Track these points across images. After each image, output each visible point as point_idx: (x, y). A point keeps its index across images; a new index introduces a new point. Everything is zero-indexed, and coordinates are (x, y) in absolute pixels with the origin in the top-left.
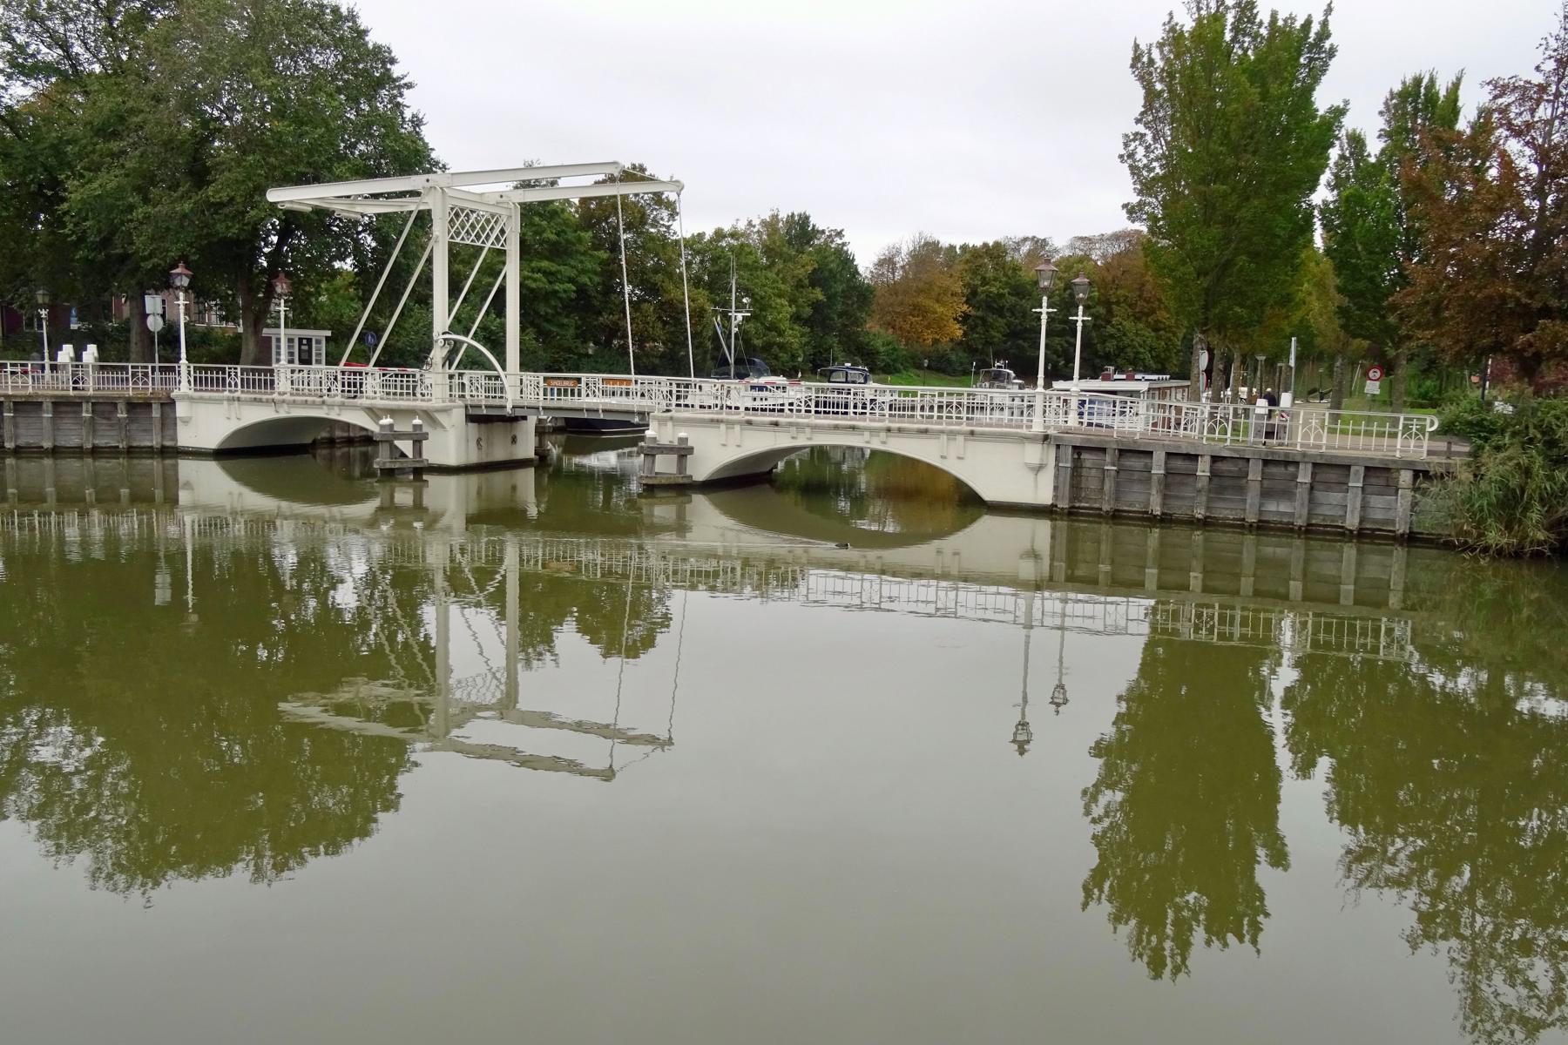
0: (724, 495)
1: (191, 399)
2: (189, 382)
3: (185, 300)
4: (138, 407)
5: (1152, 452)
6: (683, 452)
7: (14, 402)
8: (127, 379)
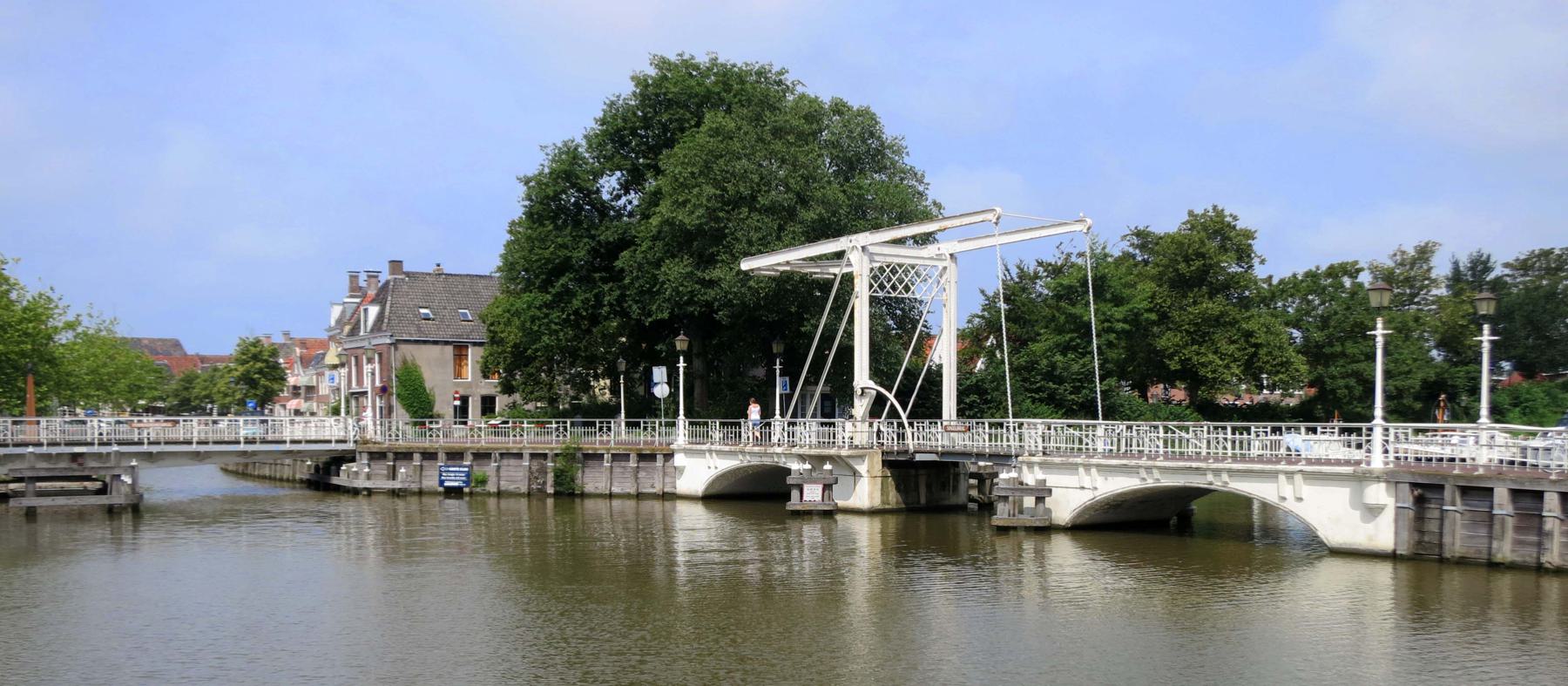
0: (1121, 537)
1: (686, 451)
2: (685, 435)
3: (1384, 329)
4: (647, 457)
5: (1491, 490)
6: (1042, 493)
7: (612, 454)
8: (595, 432)
